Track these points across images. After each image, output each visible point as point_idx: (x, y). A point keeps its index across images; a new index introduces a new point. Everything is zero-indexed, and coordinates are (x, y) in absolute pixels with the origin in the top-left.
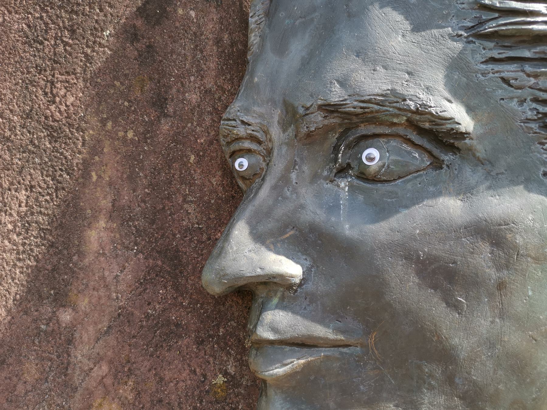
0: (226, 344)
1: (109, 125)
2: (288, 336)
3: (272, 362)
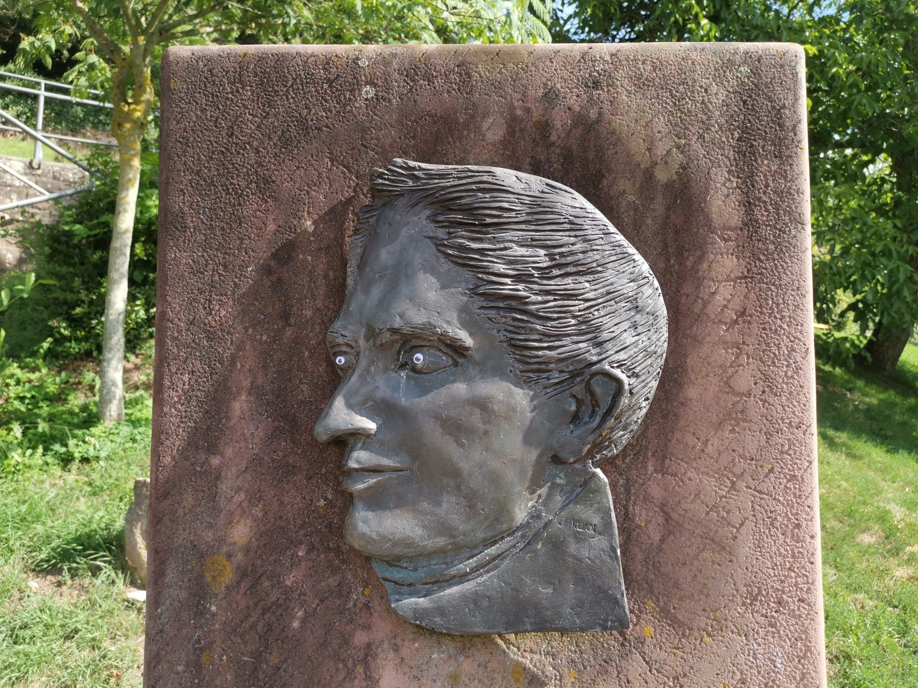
0: (327, 479)
1: (250, 331)
2: (366, 465)
3: (357, 482)
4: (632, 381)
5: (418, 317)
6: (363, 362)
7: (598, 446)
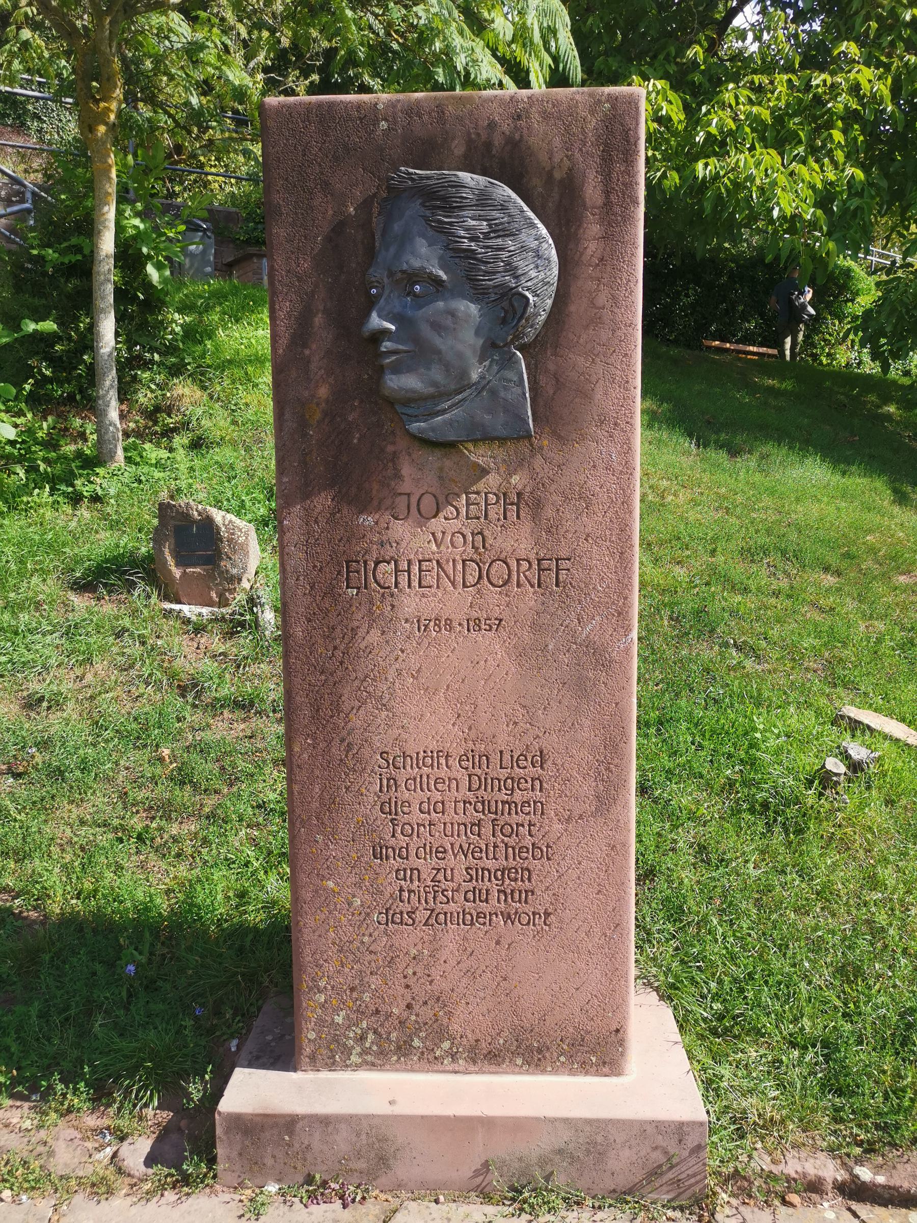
3: (386, 358)
4: (535, 299)
5: (416, 263)
6: (387, 292)
7: (516, 337)
